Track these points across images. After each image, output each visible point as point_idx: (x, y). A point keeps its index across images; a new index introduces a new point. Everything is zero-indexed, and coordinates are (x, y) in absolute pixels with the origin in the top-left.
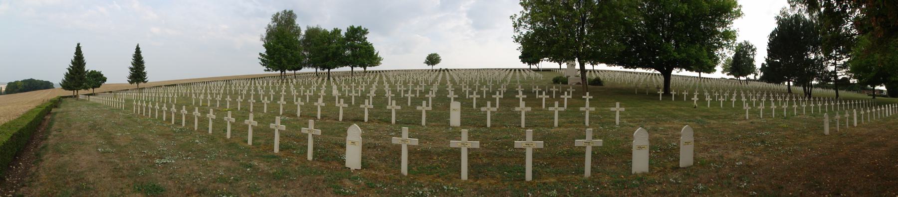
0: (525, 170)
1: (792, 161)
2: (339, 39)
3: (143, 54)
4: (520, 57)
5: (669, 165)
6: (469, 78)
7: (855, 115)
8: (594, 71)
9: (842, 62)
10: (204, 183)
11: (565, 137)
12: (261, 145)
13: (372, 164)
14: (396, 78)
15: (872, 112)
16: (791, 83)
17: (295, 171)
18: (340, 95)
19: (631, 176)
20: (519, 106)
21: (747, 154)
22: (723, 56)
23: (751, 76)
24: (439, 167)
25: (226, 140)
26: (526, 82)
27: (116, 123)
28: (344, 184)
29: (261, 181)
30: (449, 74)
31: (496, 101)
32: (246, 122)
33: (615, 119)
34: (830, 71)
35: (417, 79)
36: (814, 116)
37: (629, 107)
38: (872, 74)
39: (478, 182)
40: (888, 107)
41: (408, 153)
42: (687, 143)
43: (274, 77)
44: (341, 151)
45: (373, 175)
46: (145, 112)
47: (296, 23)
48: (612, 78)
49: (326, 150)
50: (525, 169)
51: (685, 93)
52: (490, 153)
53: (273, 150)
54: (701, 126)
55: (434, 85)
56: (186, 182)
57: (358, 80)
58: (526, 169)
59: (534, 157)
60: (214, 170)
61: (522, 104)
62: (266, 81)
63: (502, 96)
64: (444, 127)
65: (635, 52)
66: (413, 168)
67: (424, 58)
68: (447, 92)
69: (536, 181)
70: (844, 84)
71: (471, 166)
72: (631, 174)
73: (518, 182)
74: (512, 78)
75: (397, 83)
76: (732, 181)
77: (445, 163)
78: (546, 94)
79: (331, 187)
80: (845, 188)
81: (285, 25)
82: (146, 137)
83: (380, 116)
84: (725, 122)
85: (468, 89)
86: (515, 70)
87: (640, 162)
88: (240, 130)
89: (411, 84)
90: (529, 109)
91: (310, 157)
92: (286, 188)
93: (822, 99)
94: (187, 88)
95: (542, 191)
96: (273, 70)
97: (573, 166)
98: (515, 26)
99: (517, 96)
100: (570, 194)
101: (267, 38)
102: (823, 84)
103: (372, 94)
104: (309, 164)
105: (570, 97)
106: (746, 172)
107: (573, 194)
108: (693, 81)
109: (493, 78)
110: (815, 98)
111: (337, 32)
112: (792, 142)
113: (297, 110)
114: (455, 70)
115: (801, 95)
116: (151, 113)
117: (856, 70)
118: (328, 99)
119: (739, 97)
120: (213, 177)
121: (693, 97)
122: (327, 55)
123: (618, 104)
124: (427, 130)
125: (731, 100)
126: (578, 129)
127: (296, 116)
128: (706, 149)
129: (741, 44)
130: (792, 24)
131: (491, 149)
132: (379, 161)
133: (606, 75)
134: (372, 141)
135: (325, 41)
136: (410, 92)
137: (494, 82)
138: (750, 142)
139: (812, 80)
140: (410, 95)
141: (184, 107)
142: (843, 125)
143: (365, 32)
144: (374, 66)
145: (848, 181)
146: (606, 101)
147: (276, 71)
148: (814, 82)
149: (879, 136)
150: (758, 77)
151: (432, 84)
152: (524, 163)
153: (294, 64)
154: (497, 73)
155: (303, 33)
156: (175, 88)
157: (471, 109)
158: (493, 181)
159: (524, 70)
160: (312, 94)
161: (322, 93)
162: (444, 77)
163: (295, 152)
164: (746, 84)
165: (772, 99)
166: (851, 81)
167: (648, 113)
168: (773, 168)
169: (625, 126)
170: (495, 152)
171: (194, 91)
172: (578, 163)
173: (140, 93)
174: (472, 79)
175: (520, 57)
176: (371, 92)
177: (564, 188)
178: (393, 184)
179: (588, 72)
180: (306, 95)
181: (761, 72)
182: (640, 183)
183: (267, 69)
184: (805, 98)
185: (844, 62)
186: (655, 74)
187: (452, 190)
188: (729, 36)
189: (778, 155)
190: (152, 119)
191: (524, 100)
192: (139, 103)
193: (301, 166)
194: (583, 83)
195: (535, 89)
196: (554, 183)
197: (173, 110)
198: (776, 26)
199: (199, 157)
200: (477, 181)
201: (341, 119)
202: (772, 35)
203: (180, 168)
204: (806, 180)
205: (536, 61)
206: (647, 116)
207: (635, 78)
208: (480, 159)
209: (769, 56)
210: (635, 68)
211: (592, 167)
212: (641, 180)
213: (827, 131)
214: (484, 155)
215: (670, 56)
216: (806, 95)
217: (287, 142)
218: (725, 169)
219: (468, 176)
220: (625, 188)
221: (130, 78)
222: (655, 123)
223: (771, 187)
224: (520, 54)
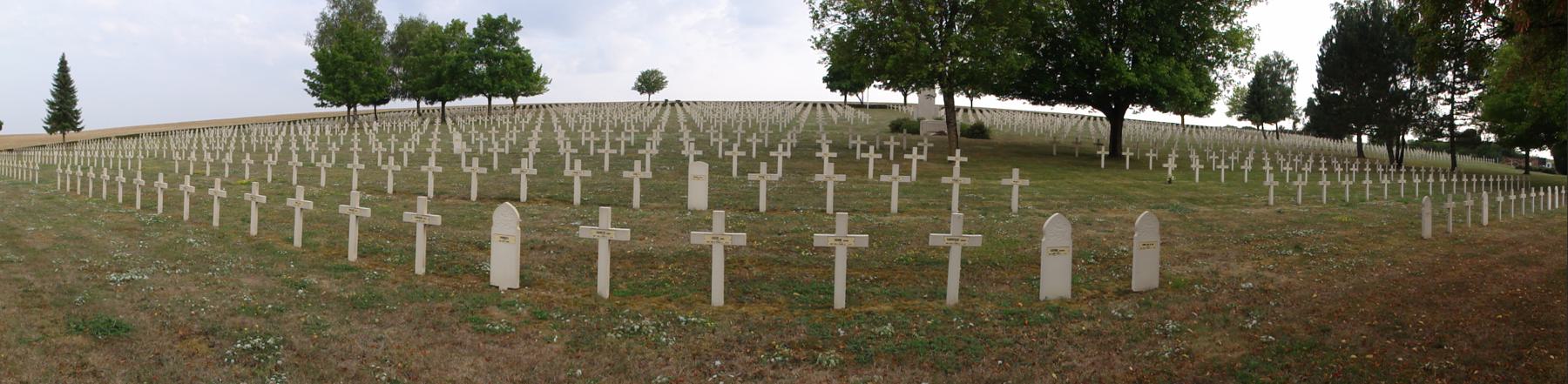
0: (833, 290)
1: (1353, 284)
2: (463, 42)
3: (72, 75)
4: (825, 80)
5: (1112, 287)
6: (724, 119)
7: (1486, 202)
8: (974, 111)
9: (1465, 98)
10: (213, 316)
11: (912, 231)
12: (322, 247)
13: (539, 277)
14: (577, 118)
15: (1518, 200)
16: (1365, 139)
17: (394, 295)
18: (470, 150)
19: (1038, 304)
20: (822, 173)
21: (1263, 270)
22: (1227, 81)
23: (1287, 124)
24: (670, 282)
25: (250, 239)
26: (838, 129)
27: (24, 209)
28: (492, 316)
29: (327, 311)
30: (684, 111)
31: (777, 164)
32: (290, 202)
33: (1010, 201)
34: (1441, 116)
35: (619, 121)
36: (1406, 203)
37: (1040, 179)
38: (1525, 125)
39: (743, 309)
40: (1553, 191)
41: (611, 258)
42: (1146, 245)
43: (334, 118)
44: (480, 257)
45: (543, 297)
46: (81, 187)
47: (377, 11)
48: (1008, 124)
49: (450, 255)
50: (832, 288)
51: (1151, 155)
52: (765, 259)
53: (347, 257)
54: (1180, 216)
55: (654, 131)
56: (176, 314)
57: (501, 122)
58: (835, 288)
59: (849, 266)
60: (231, 294)
61: (829, 168)
62: (318, 127)
63: (788, 154)
64: (677, 211)
65: (1053, 73)
66: (620, 286)
67: (633, 79)
68: (681, 147)
69: (853, 309)
70: (1469, 142)
71: (730, 281)
72: (1038, 300)
73: (820, 311)
74: (809, 119)
75: (581, 128)
76: (1230, 317)
77: (681, 276)
78: (876, 152)
79: (466, 322)
80: (1453, 337)
81: (353, 14)
82: (85, 233)
83: (550, 190)
84: (1226, 210)
85: (721, 140)
86: (815, 105)
87: (1056, 280)
88: (277, 219)
89: (607, 131)
90: (842, 178)
91: (420, 268)
92: (380, 325)
93: (1423, 170)
94: (162, 142)
95: (864, 326)
96: (333, 104)
97: (926, 283)
98: (815, 17)
99: (818, 154)
100: (918, 331)
101: (320, 40)
102: (1425, 140)
103: (533, 148)
104: (418, 282)
105: (924, 157)
106: (1258, 302)
107: (924, 333)
108: (1169, 133)
109: (770, 121)
110: (1408, 169)
111: (458, 27)
112: (1357, 249)
113: (386, 181)
114: (695, 103)
115: (1382, 162)
116: (93, 189)
117: (1494, 115)
118: (446, 159)
119: (1258, 162)
120: (231, 306)
121: (1167, 162)
122: (439, 72)
123: (1016, 172)
124: (643, 216)
125: (1242, 167)
126: (937, 219)
127: (385, 192)
128: (1186, 258)
129: (1266, 60)
130: (1367, 17)
131: (768, 251)
132: (552, 272)
133: (997, 118)
134: (538, 236)
135: (434, 45)
136: (607, 145)
137: (774, 127)
138: (1272, 248)
139: (1405, 132)
140: (607, 151)
141: (161, 176)
142: (1460, 220)
143: (515, 26)
144: (533, 94)
145: (1461, 323)
146: (995, 168)
147: (339, 105)
148: (1410, 137)
149: (1529, 245)
150: (1300, 126)
151: (649, 131)
152: (831, 278)
153: (375, 93)
154: (779, 110)
155: (391, 28)
156: (138, 141)
157: (727, 177)
158: (772, 308)
159: (832, 105)
160: (413, 150)
161: (434, 148)
162: (673, 119)
163: (389, 259)
164: (1275, 138)
165: (1323, 169)
166: (1484, 137)
167: (1077, 191)
168: (1315, 295)
169: (1029, 214)
170: (776, 257)
171: (210, 146)
172: (934, 280)
173: (68, 151)
174: (730, 121)
175: (825, 80)
176: (530, 144)
177: (908, 321)
178: (582, 313)
179: (961, 111)
180: (402, 153)
181: (1307, 115)
182: (1055, 315)
183: (320, 102)
184: (1389, 167)
185: (1471, 98)
186: (1095, 118)
187: (694, 323)
188: (1239, 40)
189: (1326, 273)
190: (95, 199)
191: (831, 159)
192: (69, 170)
193: (405, 286)
194: (948, 131)
195: (854, 142)
196: (889, 313)
197: (138, 182)
198: (1334, 23)
199: (197, 269)
200: (740, 307)
201: (474, 196)
202: (1326, 40)
203: (162, 289)
204: (1378, 320)
205: (858, 87)
206: (1073, 196)
207: (1052, 124)
208: (747, 268)
209: (1321, 82)
210: (1053, 105)
211: (962, 288)
212: (1056, 311)
213: (1427, 231)
214: (754, 261)
215: (1120, 79)
216: (1392, 162)
217: (373, 241)
218: (1220, 295)
219: (725, 299)
220: (1025, 324)
221: (49, 121)
222: (1087, 211)
223: (1307, 329)
224: (825, 73)
